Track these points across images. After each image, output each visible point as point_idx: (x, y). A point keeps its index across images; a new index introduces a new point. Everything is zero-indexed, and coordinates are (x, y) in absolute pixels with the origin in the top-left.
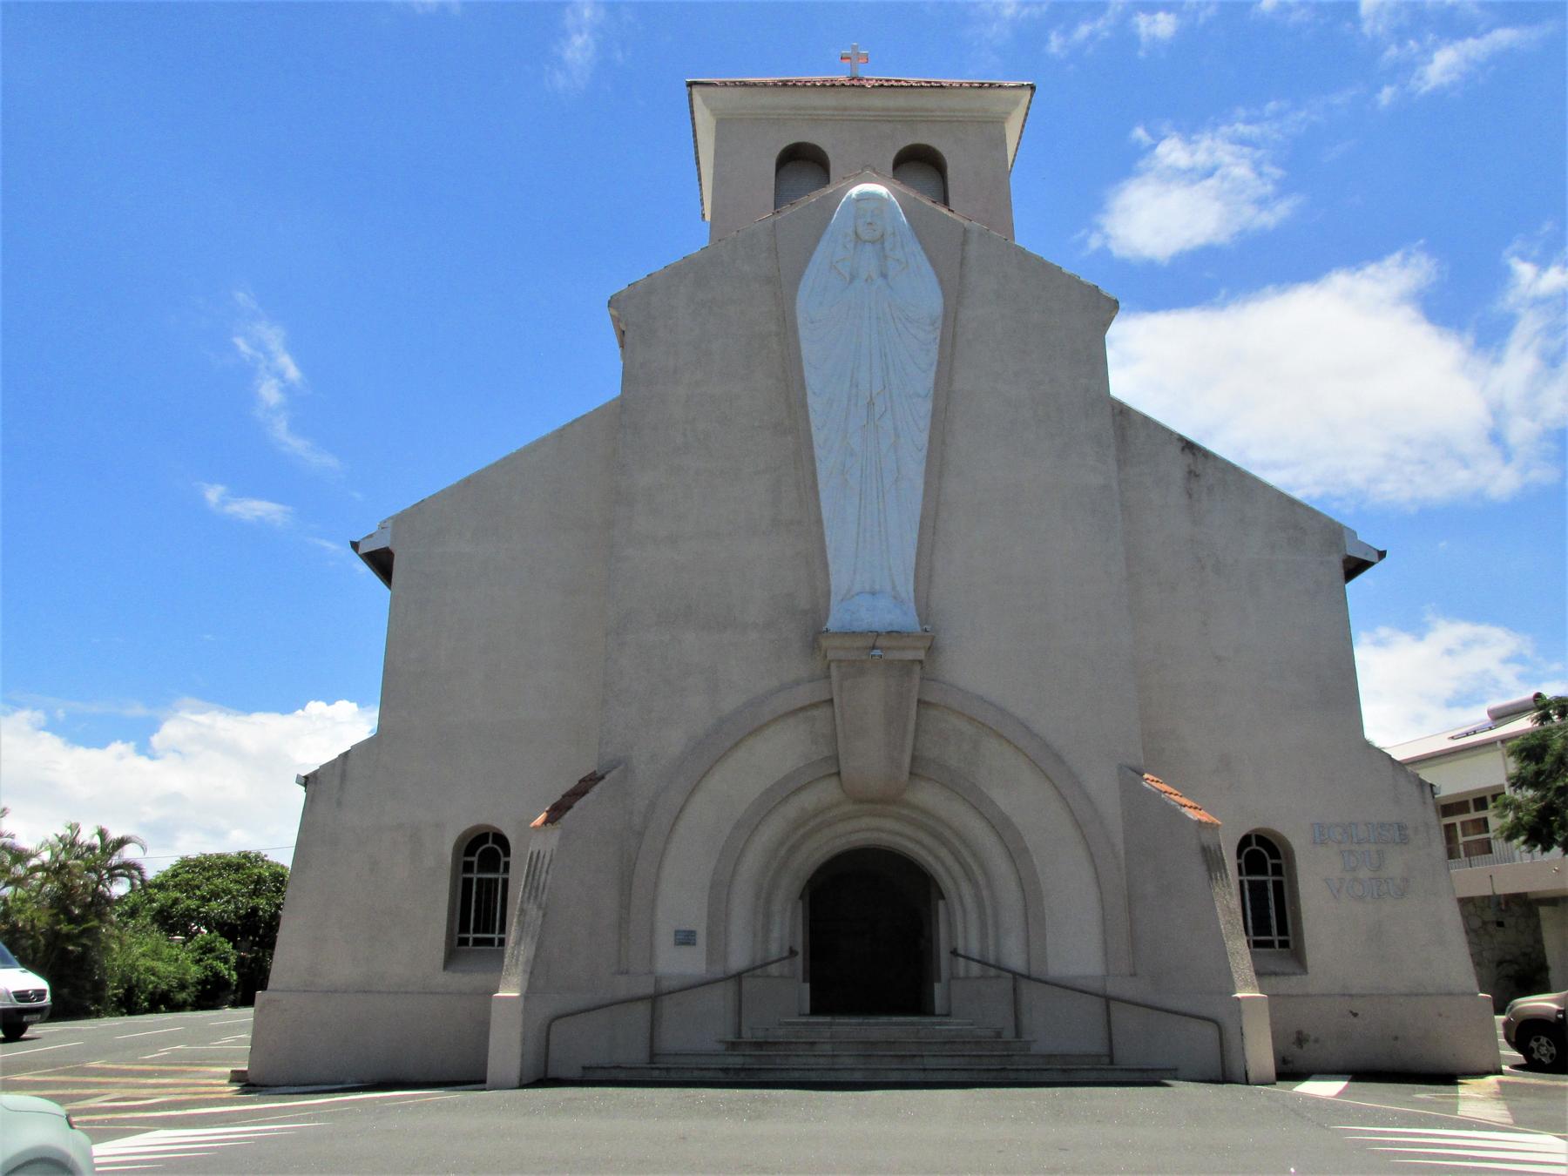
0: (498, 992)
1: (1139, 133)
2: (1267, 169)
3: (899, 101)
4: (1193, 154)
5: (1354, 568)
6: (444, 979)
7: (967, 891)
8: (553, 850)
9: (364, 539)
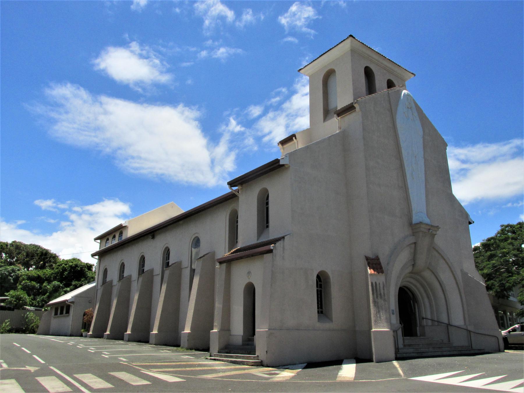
0: (213, 330)
1: (126, 36)
2: (165, 63)
3: (390, 65)
4: (142, 50)
5: (470, 223)
6: (318, 325)
7: (426, 300)
8: (383, 282)
9: (281, 159)
